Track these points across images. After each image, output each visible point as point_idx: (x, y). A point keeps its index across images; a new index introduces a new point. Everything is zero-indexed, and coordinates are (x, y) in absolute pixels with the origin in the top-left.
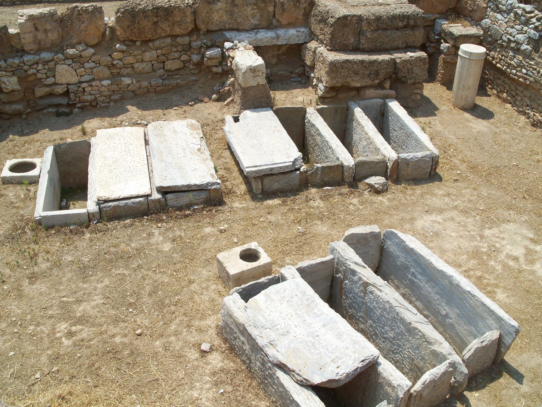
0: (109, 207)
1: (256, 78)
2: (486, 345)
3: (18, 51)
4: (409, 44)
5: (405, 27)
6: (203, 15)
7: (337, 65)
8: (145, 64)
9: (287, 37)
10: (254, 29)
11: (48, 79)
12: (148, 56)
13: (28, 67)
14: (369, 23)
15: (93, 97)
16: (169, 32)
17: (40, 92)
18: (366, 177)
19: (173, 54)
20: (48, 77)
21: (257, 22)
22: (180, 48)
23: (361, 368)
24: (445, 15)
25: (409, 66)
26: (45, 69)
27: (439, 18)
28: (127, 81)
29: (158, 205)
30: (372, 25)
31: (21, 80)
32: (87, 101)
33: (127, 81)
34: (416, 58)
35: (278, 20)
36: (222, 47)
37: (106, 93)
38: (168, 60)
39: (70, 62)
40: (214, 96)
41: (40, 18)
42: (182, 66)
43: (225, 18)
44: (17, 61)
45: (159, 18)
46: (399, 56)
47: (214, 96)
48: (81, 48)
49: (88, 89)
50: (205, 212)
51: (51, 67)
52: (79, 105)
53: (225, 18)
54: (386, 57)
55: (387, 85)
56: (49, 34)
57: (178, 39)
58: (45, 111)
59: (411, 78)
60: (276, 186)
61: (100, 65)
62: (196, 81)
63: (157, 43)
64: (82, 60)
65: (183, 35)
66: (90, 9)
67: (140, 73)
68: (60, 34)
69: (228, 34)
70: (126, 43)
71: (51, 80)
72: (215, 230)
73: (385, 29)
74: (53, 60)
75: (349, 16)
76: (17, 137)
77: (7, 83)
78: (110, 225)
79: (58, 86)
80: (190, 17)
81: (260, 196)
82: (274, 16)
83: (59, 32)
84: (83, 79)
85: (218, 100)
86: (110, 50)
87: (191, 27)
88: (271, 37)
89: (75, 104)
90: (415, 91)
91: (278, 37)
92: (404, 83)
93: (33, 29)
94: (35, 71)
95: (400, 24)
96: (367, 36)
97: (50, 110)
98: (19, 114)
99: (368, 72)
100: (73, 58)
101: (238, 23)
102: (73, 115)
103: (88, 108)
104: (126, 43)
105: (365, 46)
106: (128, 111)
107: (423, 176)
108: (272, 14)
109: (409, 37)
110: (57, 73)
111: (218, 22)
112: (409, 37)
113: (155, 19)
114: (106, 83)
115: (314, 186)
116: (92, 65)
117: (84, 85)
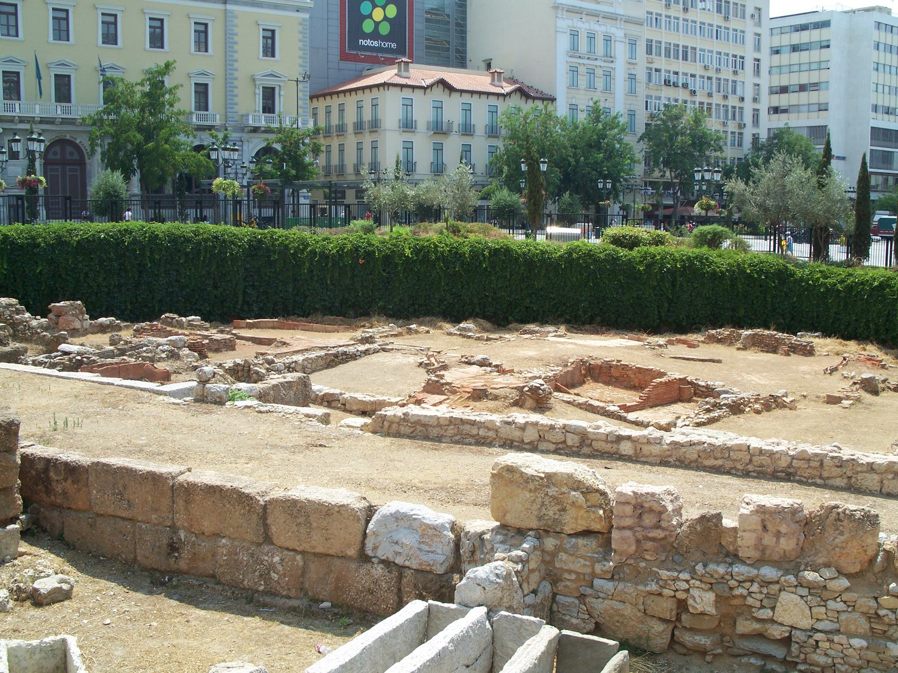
3: (727, 555)
11: (762, 611)
13: (736, 584)
17: (744, 626)
20: (763, 607)
26: (761, 592)
32: (818, 665)
37: (854, 661)
39: (804, 592)
41: (775, 512)
44: (721, 570)
48: (827, 573)
49: (824, 645)
51: (772, 592)
56: (782, 541)
58: (744, 660)
61: (854, 610)
64: (826, 594)
68: (801, 543)
71: (766, 614)
74: (777, 582)
79: (775, 626)
83: (798, 540)
84: (820, 626)
89: (797, 663)
93: (760, 528)
94: (745, 592)
97: (753, 660)
100: (811, 587)
110: (778, 604)
114: (857, 642)
116: (841, 606)
117: (818, 636)
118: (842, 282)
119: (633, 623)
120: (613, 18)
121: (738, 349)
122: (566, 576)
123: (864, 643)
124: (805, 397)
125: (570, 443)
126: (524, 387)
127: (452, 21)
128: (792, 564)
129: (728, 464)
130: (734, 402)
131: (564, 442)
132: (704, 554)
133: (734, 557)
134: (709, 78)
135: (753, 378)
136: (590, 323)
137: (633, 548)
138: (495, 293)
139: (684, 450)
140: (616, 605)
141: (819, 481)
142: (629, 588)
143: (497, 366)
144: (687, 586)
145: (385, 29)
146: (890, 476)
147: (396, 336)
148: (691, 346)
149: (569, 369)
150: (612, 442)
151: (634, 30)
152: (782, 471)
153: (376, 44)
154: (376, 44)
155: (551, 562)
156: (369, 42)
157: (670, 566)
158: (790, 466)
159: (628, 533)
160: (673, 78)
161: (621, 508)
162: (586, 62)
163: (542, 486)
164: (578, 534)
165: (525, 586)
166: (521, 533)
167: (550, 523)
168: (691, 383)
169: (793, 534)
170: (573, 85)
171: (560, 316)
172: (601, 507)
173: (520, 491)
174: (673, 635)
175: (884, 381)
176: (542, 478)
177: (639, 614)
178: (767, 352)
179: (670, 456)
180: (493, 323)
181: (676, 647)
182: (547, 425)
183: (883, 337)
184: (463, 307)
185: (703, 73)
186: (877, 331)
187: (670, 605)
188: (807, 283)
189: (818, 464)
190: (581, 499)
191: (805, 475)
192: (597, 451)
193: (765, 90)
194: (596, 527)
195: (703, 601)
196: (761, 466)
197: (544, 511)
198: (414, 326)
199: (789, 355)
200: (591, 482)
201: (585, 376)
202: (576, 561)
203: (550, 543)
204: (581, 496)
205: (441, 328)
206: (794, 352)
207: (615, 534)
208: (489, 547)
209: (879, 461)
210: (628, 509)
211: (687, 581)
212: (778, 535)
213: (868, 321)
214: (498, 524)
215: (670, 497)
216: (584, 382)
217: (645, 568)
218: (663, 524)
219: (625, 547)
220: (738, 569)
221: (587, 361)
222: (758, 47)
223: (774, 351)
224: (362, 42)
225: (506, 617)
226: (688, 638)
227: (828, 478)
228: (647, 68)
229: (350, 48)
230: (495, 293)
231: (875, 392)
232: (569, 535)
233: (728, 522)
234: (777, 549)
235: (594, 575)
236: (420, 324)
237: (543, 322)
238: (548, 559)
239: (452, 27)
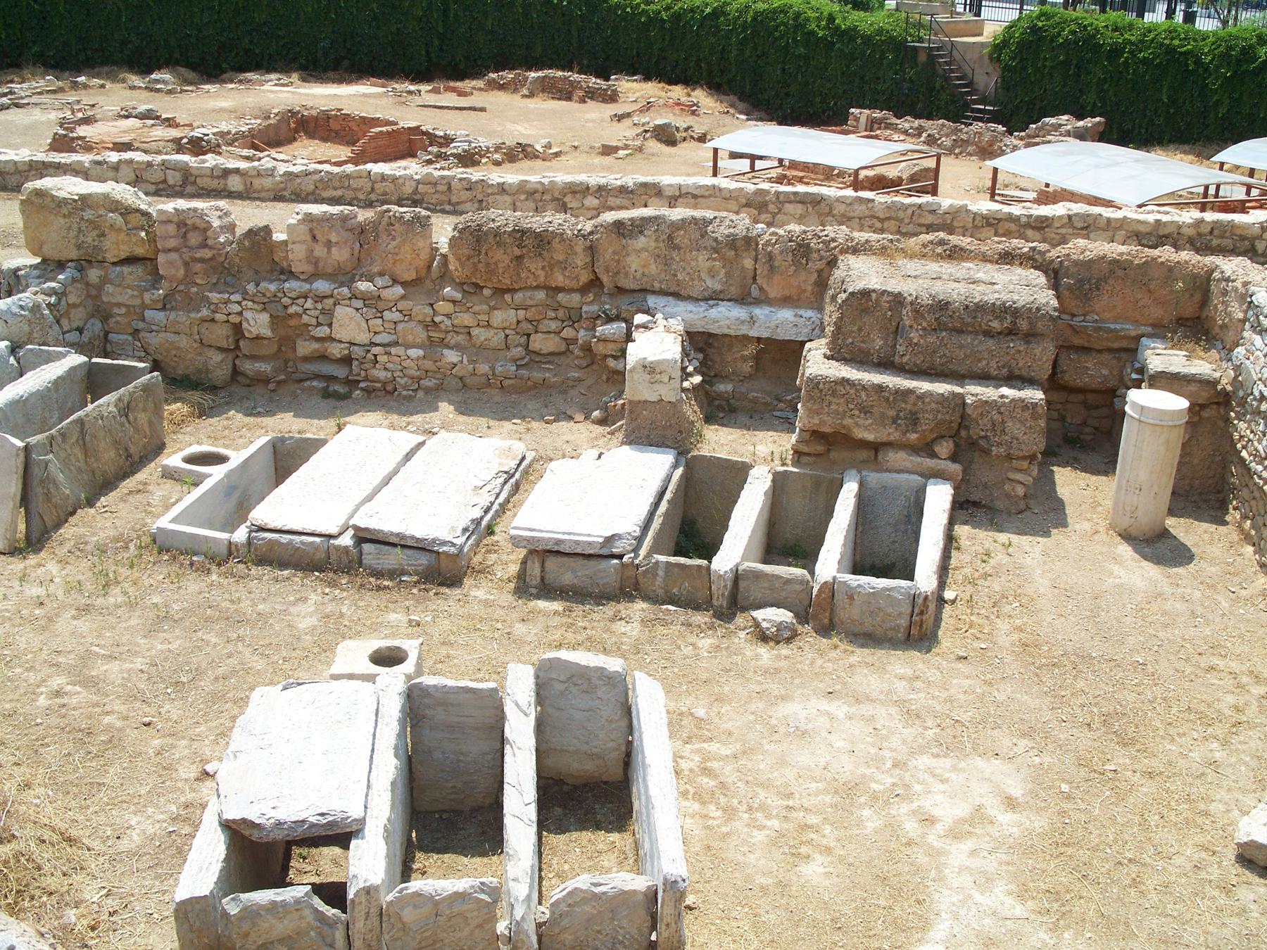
0: (263, 539)
1: (656, 386)
2: (604, 893)
3: (282, 272)
4: (1017, 372)
5: (1011, 332)
6: (607, 257)
7: (821, 386)
8: (492, 332)
9: (773, 324)
10: (711, 299)
12: (499, 317)
13: (290, 301)
14: (917, 312)
15: (389, 375)
16: (542, 279)
17: (305, 348)
18: (759, 607)
19: (546, 322)
20: (319, 324)
21: (718, 287)
22: (561, 313)
23: (313, 825)
24: (1161, 331)
25: (997, 417)
27: (1150, 336)
28: (451, 356)
29: (345, 559)
30: (925, 318)
31: (275, 321)
32: (379, 382)
33: (451, 356)
34: (1013, 400)
35: (761, 289)
36: (629, 322)
37: (413, 372)
38: (536, 332)
39: (359, 304)
40: (596, 414)
41: (322, 220)
42: (563, 348)
43: (653, 269)
44: (273, 287)
45: (524, 250)
46: (975, 392)
47: (596, 414)
48: (380, 282)
49: (381, 359)
50: (415, 591)
51: (327, 307)
52: (362, 385)
53: (653, 269)
54: (942, 388)
55: (944, 448)
56: (334, 250)
57: (560, 296)
58: (307, 384)
59: (999, 444)
60: (567, 578)
61: (411, 319)
62: (580, 380)
63: (519, 296)
64: (381, 305)
65: (571, 290)
66: (407, 216)
67: (482, 348)
68: (356, 253)
69: (652, 301)
70: (465, 287)
71: (323, 331)
72: (405, 619)
73: (960, 331)
74: (332, 296)
75: (874, 291)
76: (240, 416)
77: (252, 323)
78: (254, 571)
79: (335, 344)
80: (582, 256)
81: (534, 591)
82: (754, 278)
83: (352, 249)
84: (378, 339)
85: (602, 422)
86: (433, 296)
87: (585, 277)
88: (737, 319)
89: (359, 382)
90: (1012, 475)
91: (752, 320)
92: (987, 452)
93: (309, 238)
94: (299, 310)
95: (995, 324)
96: (911, 339)
97: (315, 383)
98: (263, 380)
99: (892, 413)
100: (366, 299)
101: (679, 283)
102: (350, 401)
103: (379, 393)
104: (465, 287)
105: (905, 359)
106: (436, 409)
107: (890, 634)
108: (752, 274)
109: (1017, 356)
111: (638, 275)
112: (1017, 356)
113: (517, 252)
114: (414, 353)
115: (646, 598)
116: (396, 316)
117: (376, 350)
118: (668, 8)
119: (190, 356)
121: (524, 96)
122: (116, 310)
123: (421, 352)
124: (576, 148)
125: (171, 182)
126: (182, 138)
128: (345, 276)
129: (349, 194)
130: (465, 151)
131: (165, 181)
132: (257, 272)
135: (519, 128)
136: (335, 69)
137: (182, 272)
138: (200, 31)
139: (298, 181)
140: (171, 337)
141: (448, 208)
142: (181, 317)
143: (168, 120)
144: (239, 309)
146: (523, 197)
147: (54, 92)
148: (461, 94)
149: (271, 122)
150: (218, 177)
152: (407, 199)
155: (98, 296)
157: (222, 288)
158: (415, 192)
159: (174, 256)
161: (163, 227)
163: (76, 209)
165: (65, 322)
166: (61, 265)
167: (90, 251)
168: (426, 133)
169: (346, 243)
171: (294, 59)
172: (143, 229)
173: (52, 217)
174: (234, 365)
175: (686, 130)
176: (75, 201)
177: (195, 345)
178: (559, 99)
179: (284, 189)
180: (201, 73)
181: (239, 378)
182: (143, 163)
183: (718, 80)
184: (156, 51)
186: (710, 73)
188: (624, 11)
189: (444, 188)
191: (433, 201)
192: (202, 189)
194: (140, 251)
195: (258, 323)
196: (385, 194)
197: (82, 238)
198: (82, 79)
199: (585, 102)
200: (130, 202)
201: (296, 131)
202: (123, 291)
203: (94, 274)
204: (120, 218)
205: (124, 81)
206: (592, 98)
207: (161, 258)
208: (24, 283)
209: (510, 181)
210: (172, 229)
211: (239, 303)
212: (329, 244)
213: (699, 60)
214: (39, 260)
215: (219, 213)
216: (295, 139)
217: (197, 293)
218: (210, 242)
219: (173, 272)
220: (293, 286)
221: (299, 112)
223: (569, 99)
225: (32, 350)
226: (248, 367)
227: (458, 203)
230: (200, 31)
231: (672, 142)
232: (114, 264)
233: (279, 236)
234: (330, 261)
235: (144, 307)
236: (98, 76)
238: (94, 294)
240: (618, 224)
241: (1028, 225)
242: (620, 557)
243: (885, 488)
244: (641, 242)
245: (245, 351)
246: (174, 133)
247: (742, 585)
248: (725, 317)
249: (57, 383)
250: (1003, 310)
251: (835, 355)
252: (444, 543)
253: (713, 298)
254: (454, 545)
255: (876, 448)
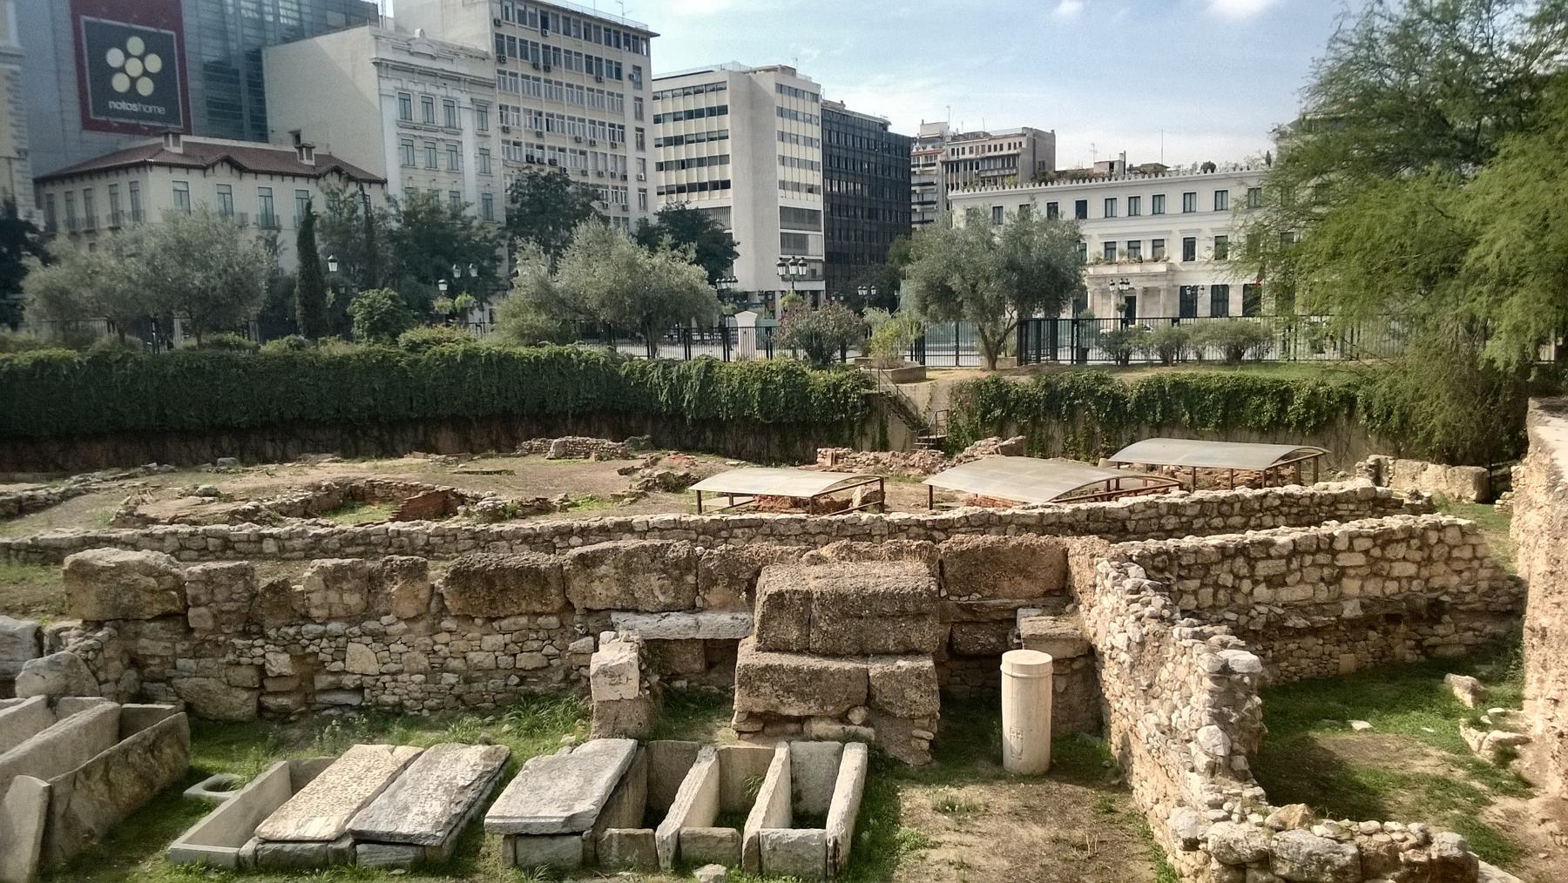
5: (903, 613)
12: (492, 641)
17: (322, 681)
21: (669, 601)
31: (298, 659)
39: (369, 640)
44: (292, 631)
46: (876, 668)
53: (616, 591)
54: (848, 665)
55: (858, 715)
63: (505, 623)
69: (614, 617)
71: (338, 666)
90: (916, 732)
91: (698, 625)
94: (316, 649)
97: (332, 711)
114: (419, 678)
116: (402, 648)
120: (456, 78)
127: (243, 77)
133: (307, 618)
134: (583, 153)
142: (209, 662)
145: (146, 87)
151: (482, 94)
153: (134, 107)
154: (134, 107)
156: (124, 105)
158: (428, 543)
160: (537, 154)
162: (422, 134)
164: (156, 619)
165: (102, 676)
166: (99, 625)
170: (408, 165)
185: (575, 146)
187: (251, 672)
190: (153, 581)
193: (651, 167)
195: (280, 662)
202: (154, 643)
222: (639, 115)
224: (113, 105)
226: (271, 701)
228: (504, 141)
229: (96, 113)
237: (317, 451)
239: (244, 85)
240: (582, 557)
241: (933, 528)
242: (580, 833)
243: (811, 755)
244: (603, 569)
245: (270, 689)
246: (230, 507)
247: (684, 847)
248: (676, 625)
249: (87, 728)
250: (890, 596)
251: (765, 647)
252: (428, 837)
253: (667, 609)
254: (435, 837)
255: (801, 720)
